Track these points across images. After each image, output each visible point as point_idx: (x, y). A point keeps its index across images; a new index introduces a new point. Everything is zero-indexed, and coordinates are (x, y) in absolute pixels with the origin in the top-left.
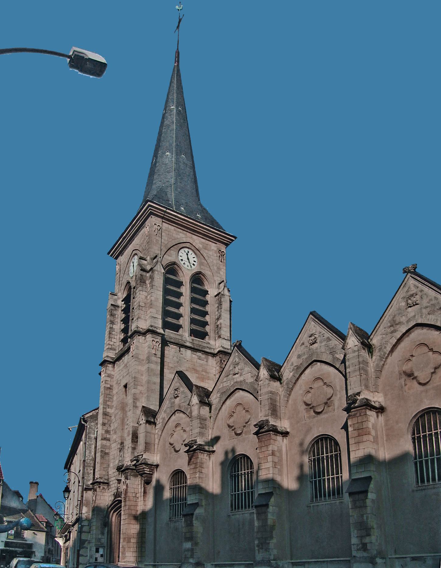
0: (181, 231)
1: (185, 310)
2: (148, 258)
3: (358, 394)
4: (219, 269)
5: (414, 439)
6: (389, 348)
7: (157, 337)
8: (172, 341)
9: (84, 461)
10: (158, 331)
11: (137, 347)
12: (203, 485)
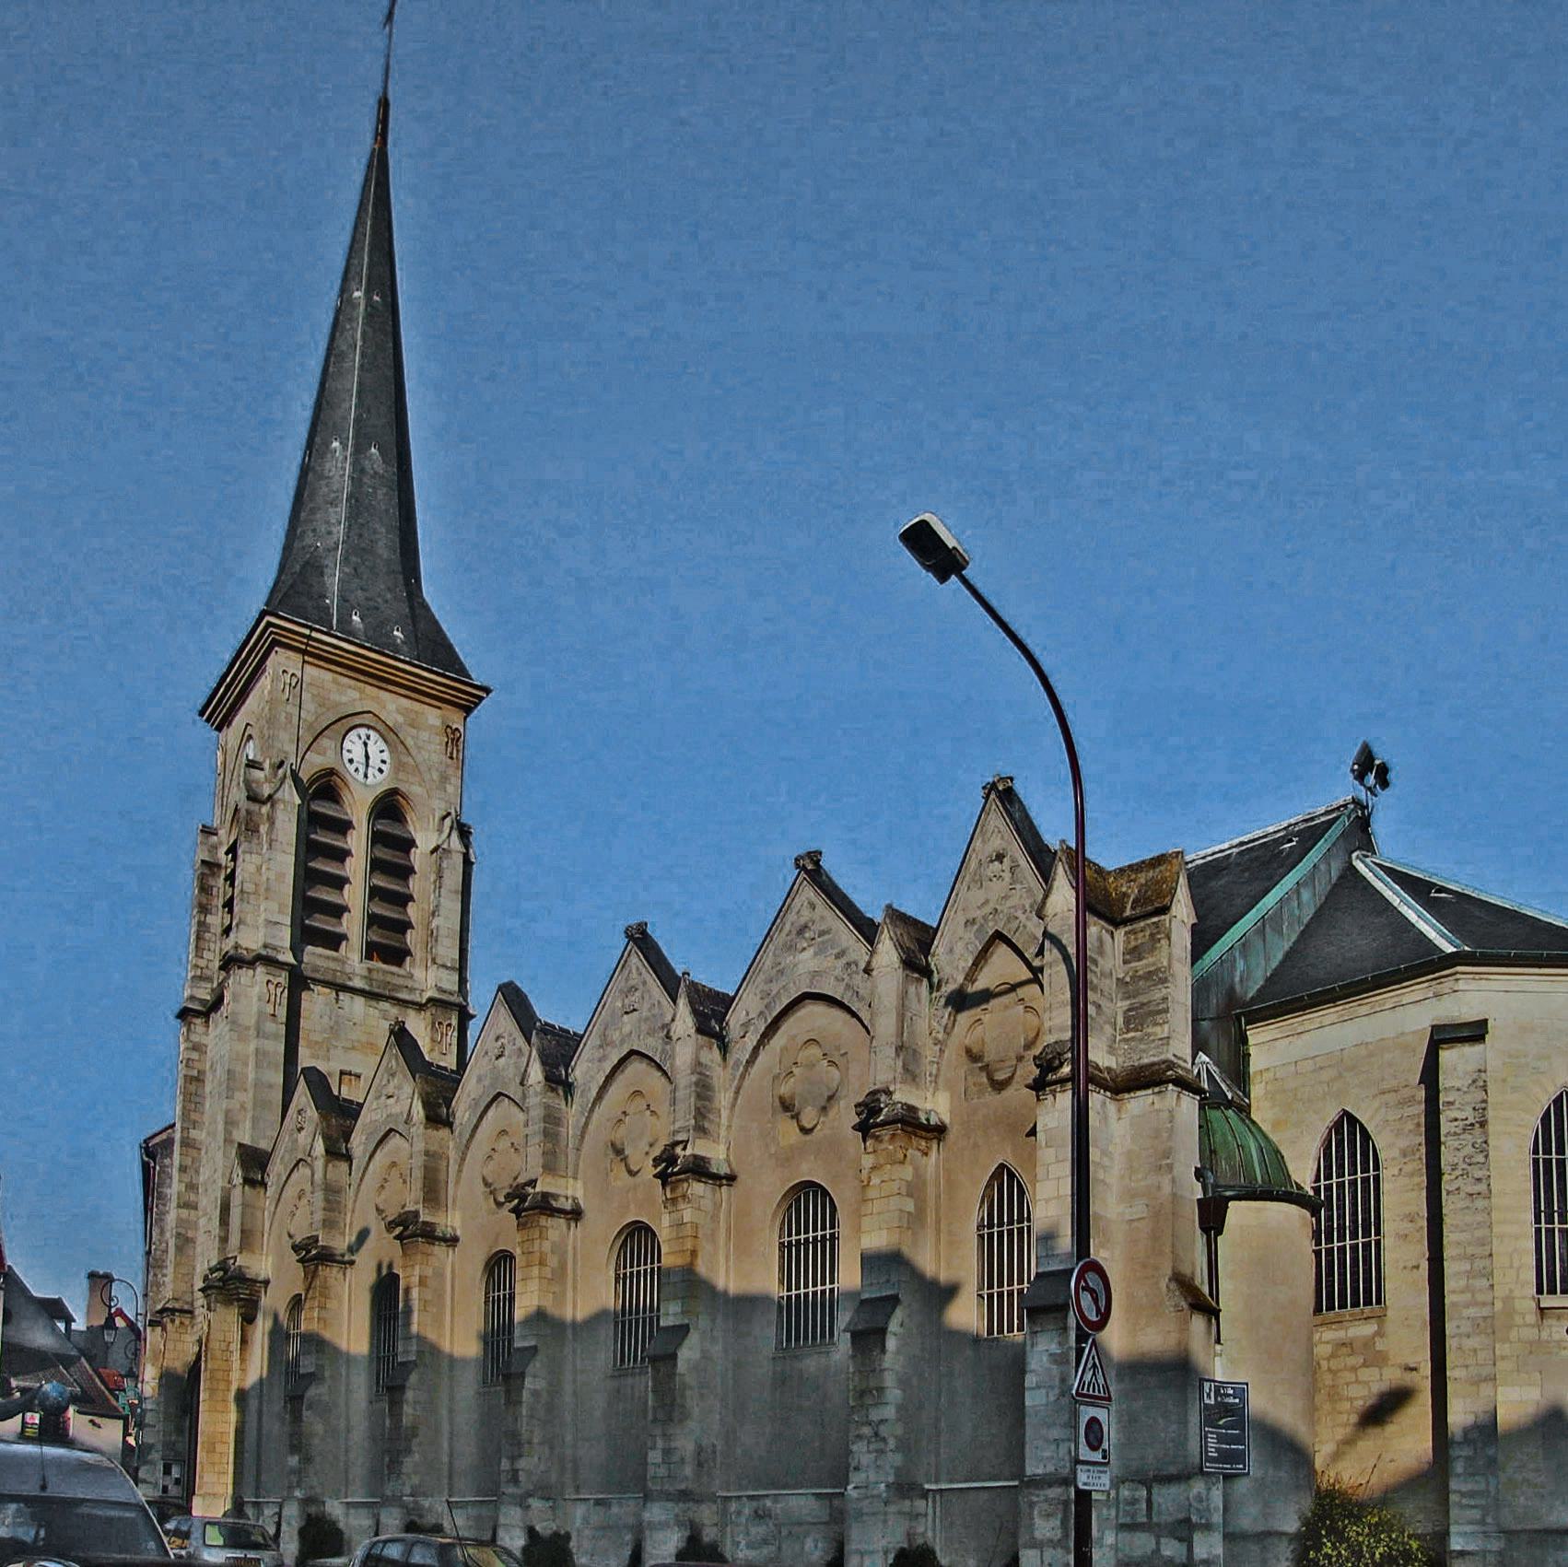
0: (352, 682)
1: (354, 896)
2: (266, 765)
3: (533, 1183)
4: (444, 779)
6: (594, 1093)
7: (277, 972)
8: (318, 976)
9: (148, 1253)
10: (281, 958)
11: (235, 998)
12: (327, 1335)
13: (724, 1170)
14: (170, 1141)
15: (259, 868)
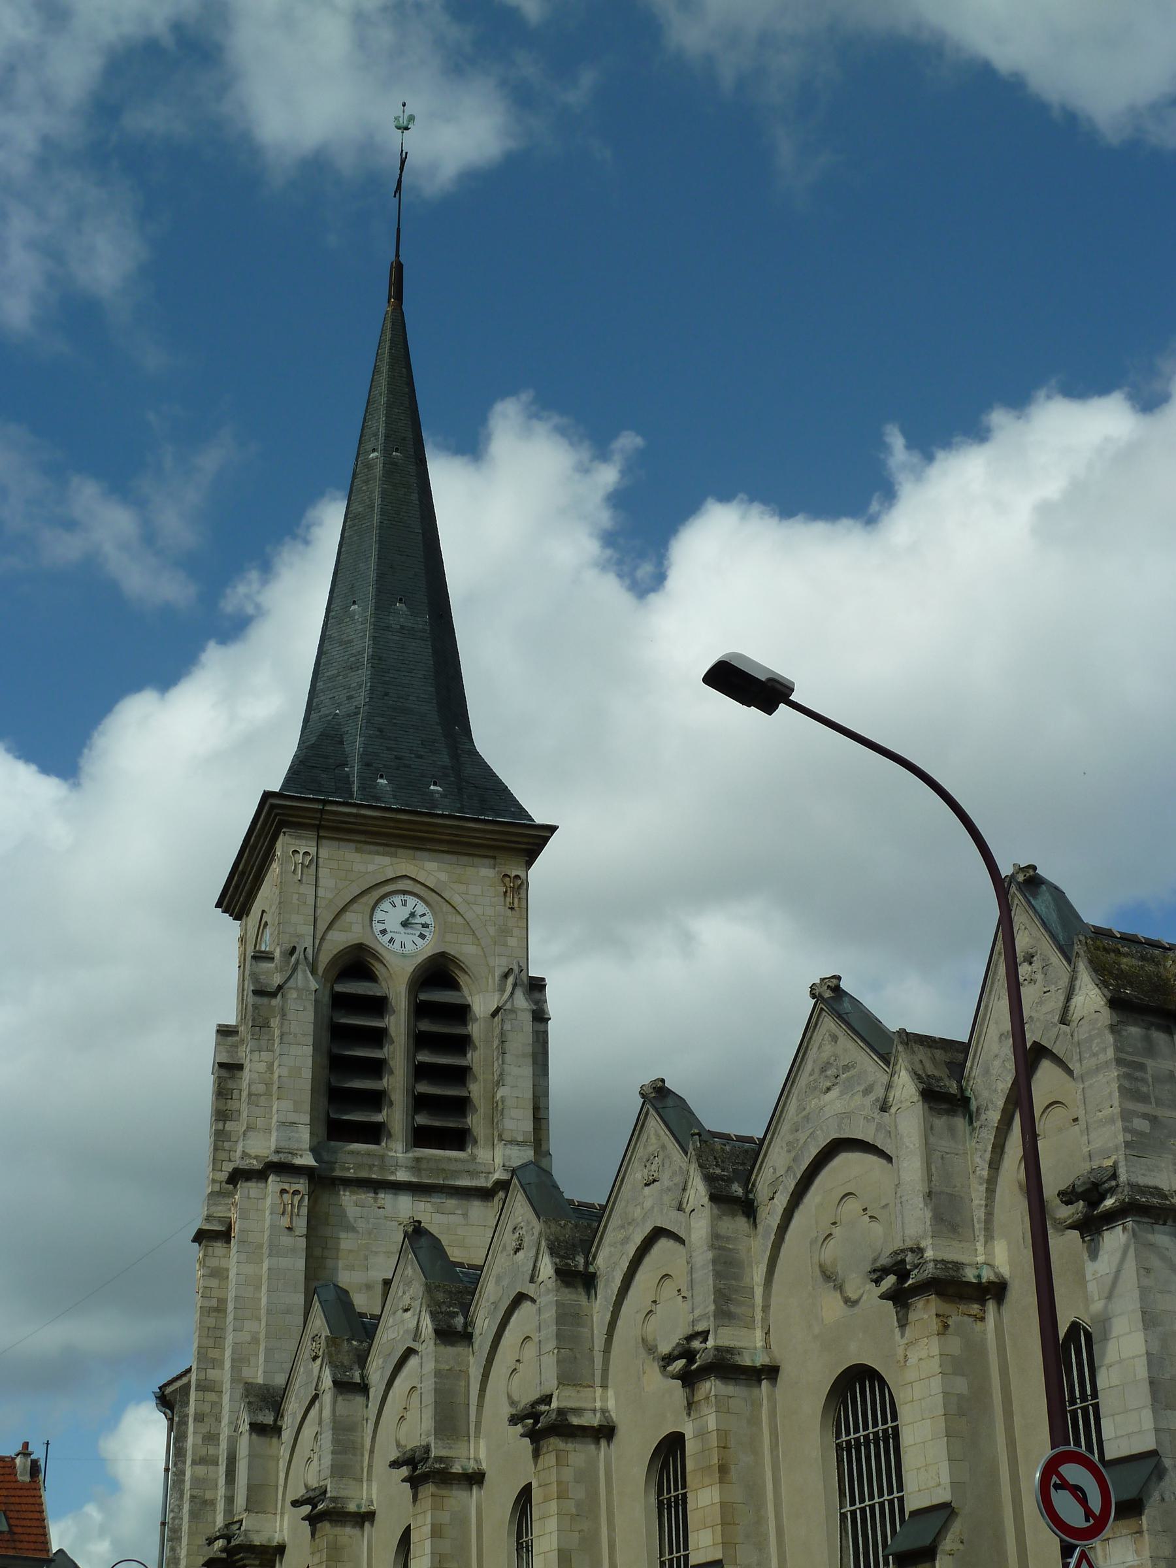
2: (277, 954)
3: (547, 1399)
5: (660, 1503)
10: (298, 1161)
13: (761, 1360)
14: (187, 1387)
15: (270, 1066)
